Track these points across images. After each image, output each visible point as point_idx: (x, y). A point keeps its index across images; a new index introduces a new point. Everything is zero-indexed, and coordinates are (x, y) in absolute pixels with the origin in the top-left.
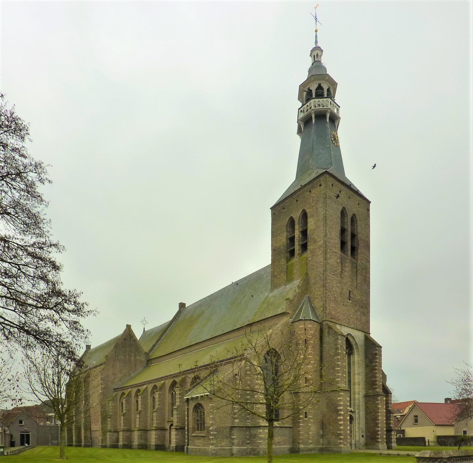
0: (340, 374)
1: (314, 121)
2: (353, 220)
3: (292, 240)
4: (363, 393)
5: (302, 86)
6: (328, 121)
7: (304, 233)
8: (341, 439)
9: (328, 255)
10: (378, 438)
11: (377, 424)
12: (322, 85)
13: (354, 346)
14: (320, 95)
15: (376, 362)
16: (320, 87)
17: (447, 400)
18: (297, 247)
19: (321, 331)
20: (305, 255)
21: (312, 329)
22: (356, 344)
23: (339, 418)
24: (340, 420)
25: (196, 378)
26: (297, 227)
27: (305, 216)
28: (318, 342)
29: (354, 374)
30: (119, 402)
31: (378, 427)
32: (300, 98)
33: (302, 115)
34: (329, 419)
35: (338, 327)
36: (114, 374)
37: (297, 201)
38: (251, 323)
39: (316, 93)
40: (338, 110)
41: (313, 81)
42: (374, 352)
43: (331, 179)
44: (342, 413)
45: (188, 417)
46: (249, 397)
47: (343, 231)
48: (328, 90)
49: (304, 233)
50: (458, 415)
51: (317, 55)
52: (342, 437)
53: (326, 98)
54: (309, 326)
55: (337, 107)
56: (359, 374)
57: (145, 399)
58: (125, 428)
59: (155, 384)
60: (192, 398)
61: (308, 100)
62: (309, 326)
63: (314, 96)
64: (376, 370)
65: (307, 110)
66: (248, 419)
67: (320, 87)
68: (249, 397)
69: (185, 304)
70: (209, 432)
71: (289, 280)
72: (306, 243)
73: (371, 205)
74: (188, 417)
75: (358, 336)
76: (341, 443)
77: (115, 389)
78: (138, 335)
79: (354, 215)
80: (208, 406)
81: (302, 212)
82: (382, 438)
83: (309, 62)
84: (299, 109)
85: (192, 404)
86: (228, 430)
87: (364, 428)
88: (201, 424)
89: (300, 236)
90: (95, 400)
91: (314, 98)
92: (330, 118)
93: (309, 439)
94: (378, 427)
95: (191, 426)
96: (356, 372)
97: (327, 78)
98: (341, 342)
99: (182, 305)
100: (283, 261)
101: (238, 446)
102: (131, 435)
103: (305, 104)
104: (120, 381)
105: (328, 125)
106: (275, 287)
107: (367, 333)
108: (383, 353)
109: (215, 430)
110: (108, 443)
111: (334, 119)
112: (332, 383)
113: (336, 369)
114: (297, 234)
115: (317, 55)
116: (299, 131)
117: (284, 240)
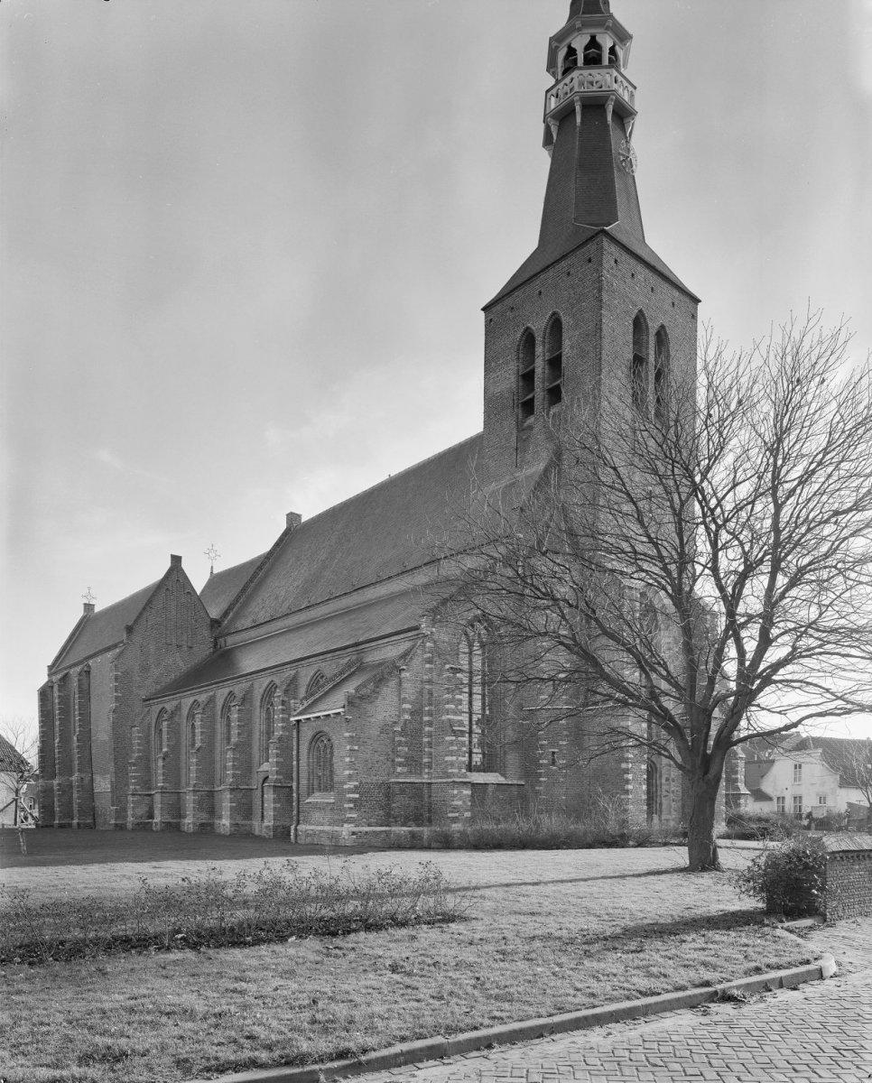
1: (578, 120)
7: (555, 363)
16: (593, 43)
26: (539, 350)
27: (556, 326)
33: (553, 103)
39: (585, 57)
40: (632, 96)
41: (579, 29)
45: (298, 761)
48: (612, 51)
49: (555, 363)
55: (631, 89)
67: (593, 43)
81: (551, 317)
91: (581, 68)
100: (509, 425)
103: (563, 79)
111: (624, 114)
114: (540, 366)
117: (513, 378)
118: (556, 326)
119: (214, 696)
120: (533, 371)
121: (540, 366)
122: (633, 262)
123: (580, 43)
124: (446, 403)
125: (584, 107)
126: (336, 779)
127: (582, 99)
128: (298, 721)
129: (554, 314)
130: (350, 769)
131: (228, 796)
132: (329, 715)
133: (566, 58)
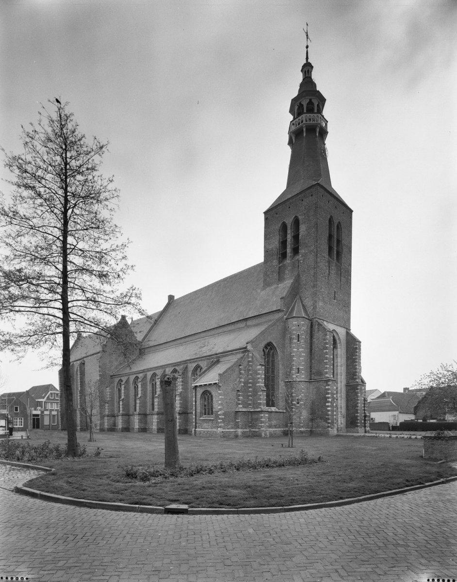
0: (328, 366)
1: (305, 135)
2: (339, 227)
3: (284, 243)
4: (344, 382)
5: (294, 101)
6: (317, 135)
7: (296, 237)
8: (329, 423)
9: (319, 259)
10: (358, 423)
11: (357, 410)
12: (313, 101)
13: (338, 340)
14: (310, 110)
15: (356, 355)
16: (310, 103)
17: (405, 389)
18: (289, 250)
19: (312, 326)
20: (297, 257)
21: (304, 326)
22: (339, 339)
23: (327, 404)
24: (328, 406)
25: (198, 367)
26: (289, 231)
27: (296, 222)
28: (308, 337)
29: (337, 366)
30: (115, 388)
31: (358, 413)
32: (291, 111)
33: (293, 128)
34: (318, 405)
35: (325, 323)
36: (110, 362)
37: (289, 207)
38: (247, 318)
39: (307, 108)
40: (326, 125)
41: (305, 96)
42: (355, 347)
43: (321, 190)
44: (330, 400)
45: (196, 402)
46: (251, 385)
47: (330, 237)
48: (318, 106)
49: (296, 237)
50: (142, 429)
51: (308, 71)
52: (330, 421)
53: (316, 113)
54: (302, 323)
55: (326, 122)
56: (341, 366)
57: (144, 386)
58: (124, 412)
59: (154, 371)
60: (201, 386)
61: (299, 114)
62: (302, 323)
63: (305, 111)
64: (356, 362)
65: (299, 124)
66: (250, 405)
67: (310, 103)
68: (251, 385)
69: (173, 297)
70: (217, 416)
71: (281, 279)
72: (298, 247)
73: (353, 214)
74: (196, 402)
75: (341, 332)
76: (328, 427)
77: (111, 376)
78: (129, 322)
79: (339, 222)
80: (215, 392)
81: (294, 218)
82: (361, 423)
83: (300, 78)
84: (291, 122)
85: (200, 391)
86: (233, 414)
87: (345, 414)
88: (209, 409)
89: (292, 240)
90: (91, 388)
91: (305, 113)
92: (319, 133)
93: (300, 423)
94: (358, 413)
95: (198, 411)
96: (339, 364)
97: (317, 94)
98: (329, 337)
99: (171, 297)
100: (275, 262)
101: (242, 429)
102: (129, 418)
103: (297, 118)
104: (116, 368)
105: (318, 139)
106: (268, 286)
107: (348, 329)
108: (362, 347)
109: (223, 414)
110: (106, 426)
111: (323, 133)
112: (320, 373)
113: (325, 361)
114: (289, 237)
115: (308, 71)
116: (290, 143)
117: (277, 243)
118: (296, 222)
119: (146, 374)
120: (286, 240)
121: (289, 237)
122: (329, 196)
123: (305, 103)
124: (248, 249)
125: (306, 129)
126: (214, 410)
127: (306, 126)
128: (196, 386)
129: (296, 217)
130: (327, 347)
131: (156, 417)
132: (206, 384)
133: (298, 109)
